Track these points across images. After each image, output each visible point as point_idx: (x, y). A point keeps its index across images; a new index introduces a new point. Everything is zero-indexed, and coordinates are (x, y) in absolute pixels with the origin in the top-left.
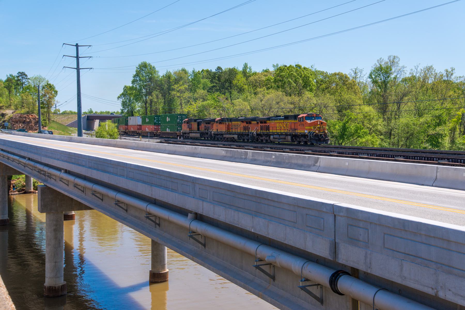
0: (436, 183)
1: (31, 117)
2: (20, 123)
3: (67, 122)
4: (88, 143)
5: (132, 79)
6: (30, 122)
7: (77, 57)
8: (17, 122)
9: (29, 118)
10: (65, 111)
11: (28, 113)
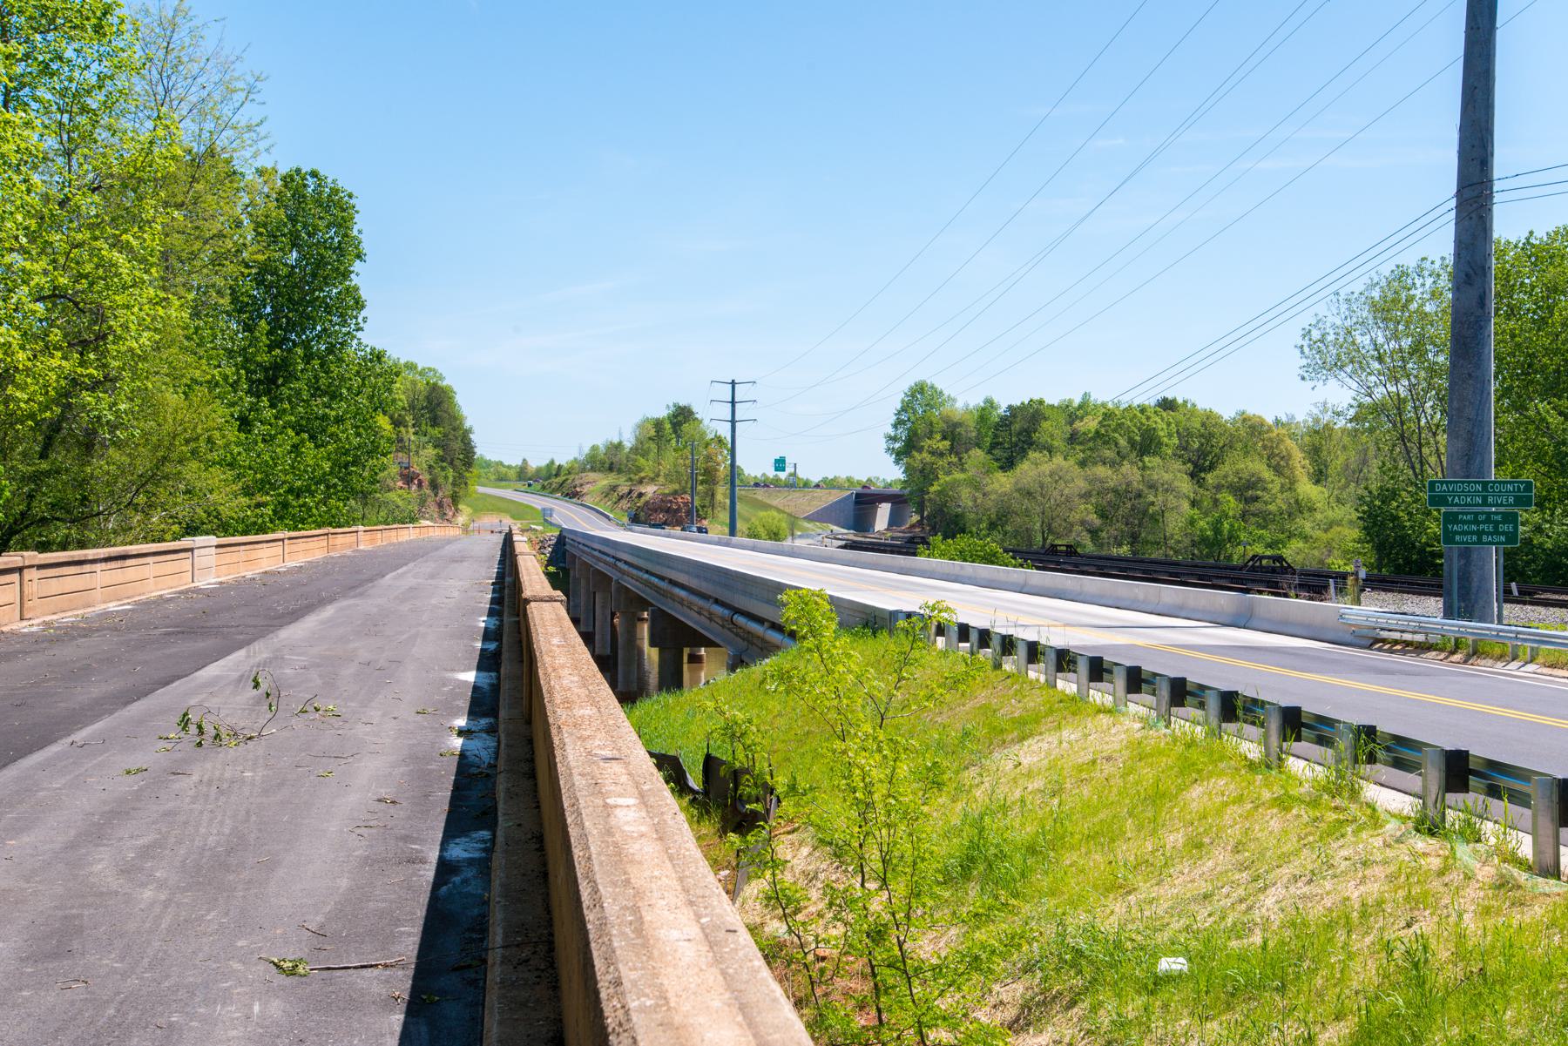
0: (1022, 589)
1: (680, 500)
2: (661, 511)
3: (808, 508)
4: (1110, 603)
5: (893, 419)
6: (679, 510)
7: (733, 403)
8: (656, 511)
9: (677, 503)
10: (869, 480)
11: (675, 493)
